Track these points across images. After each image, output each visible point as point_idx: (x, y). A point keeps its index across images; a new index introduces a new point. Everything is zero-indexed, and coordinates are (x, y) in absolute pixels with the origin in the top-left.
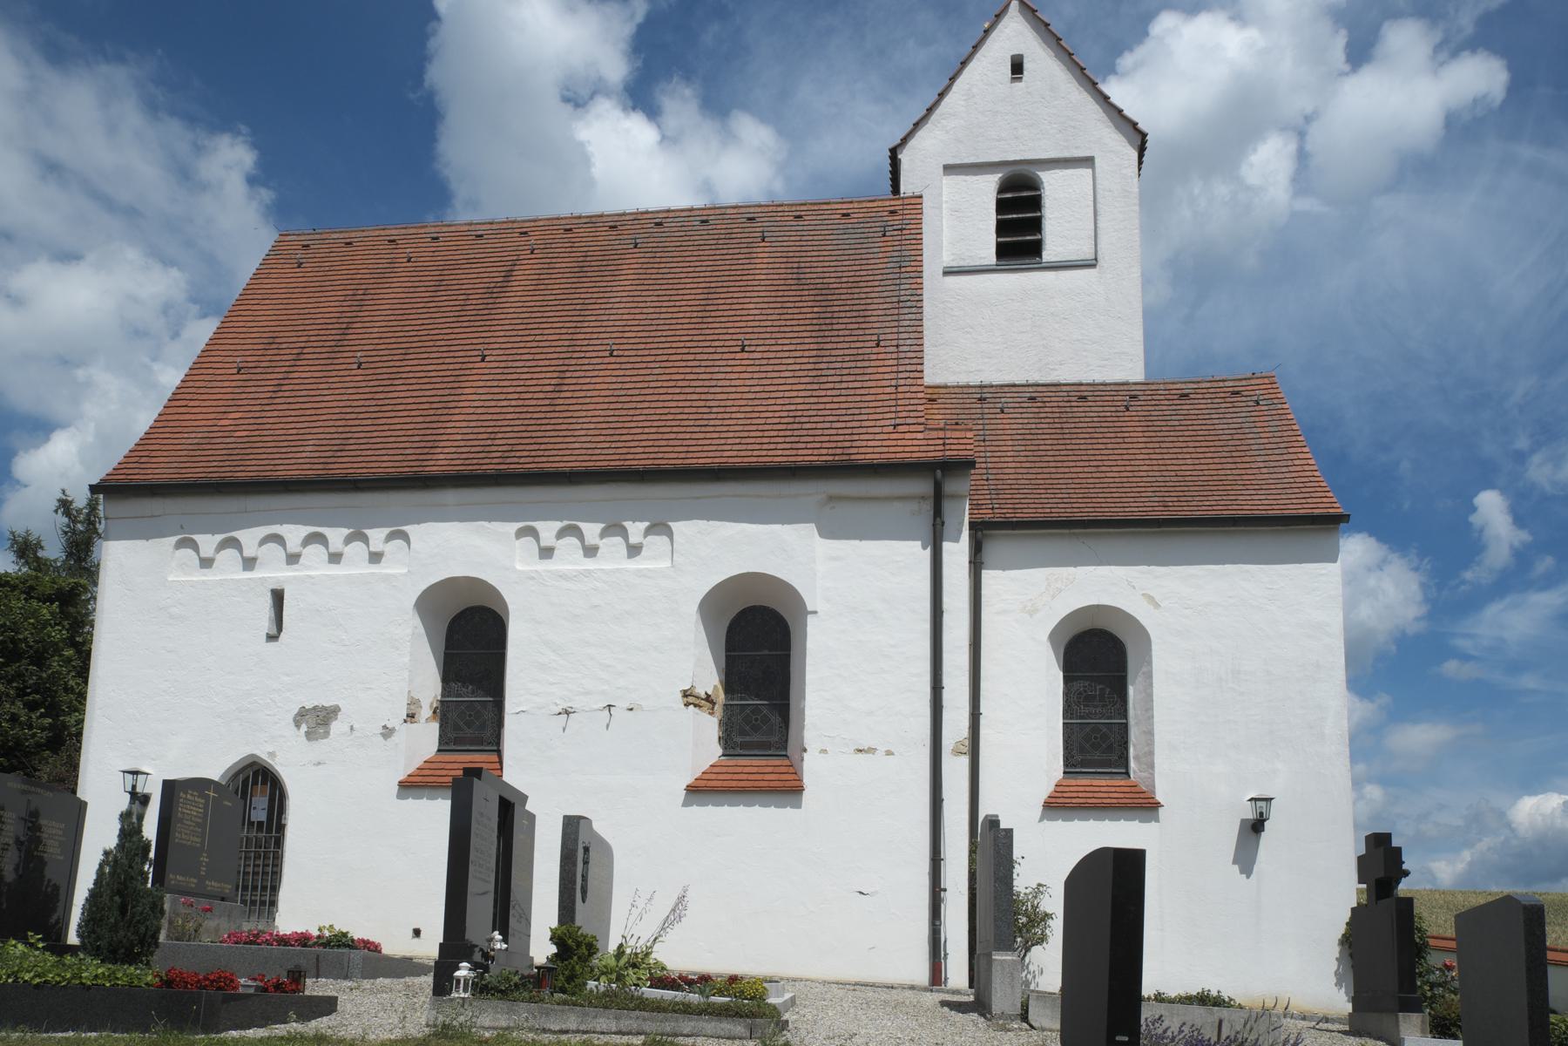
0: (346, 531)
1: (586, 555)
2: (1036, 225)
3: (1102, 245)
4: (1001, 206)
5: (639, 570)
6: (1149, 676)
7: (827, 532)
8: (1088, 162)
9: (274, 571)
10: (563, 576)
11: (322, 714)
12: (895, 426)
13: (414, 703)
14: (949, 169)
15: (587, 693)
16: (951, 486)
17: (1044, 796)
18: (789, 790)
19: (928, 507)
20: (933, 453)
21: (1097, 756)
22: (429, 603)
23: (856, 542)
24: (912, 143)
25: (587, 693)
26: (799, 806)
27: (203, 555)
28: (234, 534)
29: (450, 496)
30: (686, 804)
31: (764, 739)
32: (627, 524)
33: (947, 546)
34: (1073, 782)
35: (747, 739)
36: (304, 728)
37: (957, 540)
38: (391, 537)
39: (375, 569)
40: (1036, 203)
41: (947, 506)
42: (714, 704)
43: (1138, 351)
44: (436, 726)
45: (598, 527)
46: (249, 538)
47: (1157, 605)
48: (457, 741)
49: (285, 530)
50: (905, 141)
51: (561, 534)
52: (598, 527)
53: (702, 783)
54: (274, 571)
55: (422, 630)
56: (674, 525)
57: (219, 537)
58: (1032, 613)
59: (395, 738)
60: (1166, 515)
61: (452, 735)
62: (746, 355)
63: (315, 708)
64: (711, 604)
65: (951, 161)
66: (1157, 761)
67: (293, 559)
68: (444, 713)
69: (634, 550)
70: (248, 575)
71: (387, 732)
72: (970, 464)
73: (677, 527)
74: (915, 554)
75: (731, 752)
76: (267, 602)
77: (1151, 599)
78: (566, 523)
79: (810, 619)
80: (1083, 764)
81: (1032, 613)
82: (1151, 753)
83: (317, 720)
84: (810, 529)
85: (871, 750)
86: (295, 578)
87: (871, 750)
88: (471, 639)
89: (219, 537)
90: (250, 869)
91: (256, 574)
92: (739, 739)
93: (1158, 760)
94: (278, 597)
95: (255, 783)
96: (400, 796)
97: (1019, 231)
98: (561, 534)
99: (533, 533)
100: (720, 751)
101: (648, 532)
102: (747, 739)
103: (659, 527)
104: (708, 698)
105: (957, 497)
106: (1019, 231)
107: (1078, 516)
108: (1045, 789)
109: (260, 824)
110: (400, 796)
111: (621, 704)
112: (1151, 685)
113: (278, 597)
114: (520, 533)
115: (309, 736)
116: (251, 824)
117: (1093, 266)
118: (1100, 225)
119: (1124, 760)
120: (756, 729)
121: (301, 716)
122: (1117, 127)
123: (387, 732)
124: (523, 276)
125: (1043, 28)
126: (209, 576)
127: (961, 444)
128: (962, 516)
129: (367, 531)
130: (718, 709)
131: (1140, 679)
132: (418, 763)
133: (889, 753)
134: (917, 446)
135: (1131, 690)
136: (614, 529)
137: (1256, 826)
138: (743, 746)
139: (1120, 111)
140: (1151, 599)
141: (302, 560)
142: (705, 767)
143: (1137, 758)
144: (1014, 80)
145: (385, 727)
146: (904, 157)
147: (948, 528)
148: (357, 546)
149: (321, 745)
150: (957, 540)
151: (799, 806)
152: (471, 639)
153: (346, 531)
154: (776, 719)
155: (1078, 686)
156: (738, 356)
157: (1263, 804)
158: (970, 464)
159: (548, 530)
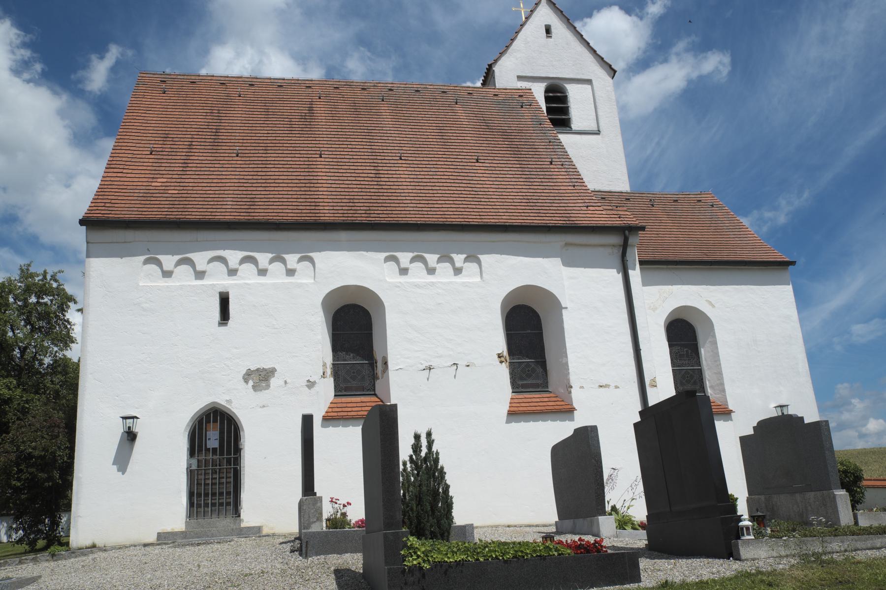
0: (270, 256)
1: (259, 274)
2: (565, 111)
5: (464, 283)
6: (715, 343)
7: (567, 263)
8: (589, 82)
9: (218, 280)
10: (417, 286)
11: (263, 374)
12: (587, 207)
15: (440, 357)
16: (633, 240)
17: (506, 412)
19: (618, 252)
23: (582, 269)
24: (500, 62)
25: (440, 357)
26: (573, 420)
27: (289, 267)
28: (311, 254)
29: (343, 236)
30: (507, 422)
31: (534, 382)
32: (454, 256)
33: (631, 272)
35: (525, 382)
36: (251, 383)
37: (634, 269)
38: (301, 260)
39: (290, 280)
40: (564, 99)
41: (629, 250)
43: (625, 178)
44: (332, 379)
45: (435, 257)
46: (201, 258)
47: (713, 306)
48: (346, 389)
49: (228, 254)
50: (496, 61)
51: (413, 260)
52: (435, 257)
54: (218, 280)
55: (324, 319)
56: (482, 257)
57: (177, 257)
61: (343, 385)
63: (258, 370)
67: (232, 272)
68: (337, 372)
69: (458, 271)
70: (199, 282)
71: (311, 384)
73: (483, 258)
74: (614, 276)
78: (416, 254)
79: (564, 311)
82: (722, 384)
83: (260, 378)
84: (557, 261)
85: (607, 386)
86: (236, 284)
87: (607, 386)
88: (354, 327)
89: (177, 257)
90: (210, 482)
91: (206, 282)
92: (521, 383)
93: (727, 387)
94: (224, 301)
95: (208, 422)
98: (413, 260)
99: (395, 259)
101: (466, 260)
102: (525, 382)
103: (472, 258)
107: (671, 258)
109: (214, 450)
111: (462, 363)
112: (717, 348)
113: (224, 301)
114: (387, 259)
115: (255, 388)
116: (208, 450)
117: (598, 134)
120: (529, 376)
121: (248, 375)
122: (601, 66)
123: (311, 384)
124: (320, 109)
125: (559, 12)
126: (459, 279)
127: (629, 219)
128: (634, 255)
129: (285, 256)
131: (708, 345)
133: (617, 387)
134: (601, 216)
135: (702, 351)
136: (445, 258)
137: (131, 436)
138: (523, 386)
139: (602, 59)
141: (239, 273)
143: (711, 387)
144: (548, 37)
145: (308, 381)
146: (496, 69)
147: (629, 264)
148: (278, 265)
149: (264, 395)
150: (634, 269)
152: (354, 327)
153: (270, 256)
154: (539, 370)
155: (676, 349)
156: (477, 164)
159: (405, 258)
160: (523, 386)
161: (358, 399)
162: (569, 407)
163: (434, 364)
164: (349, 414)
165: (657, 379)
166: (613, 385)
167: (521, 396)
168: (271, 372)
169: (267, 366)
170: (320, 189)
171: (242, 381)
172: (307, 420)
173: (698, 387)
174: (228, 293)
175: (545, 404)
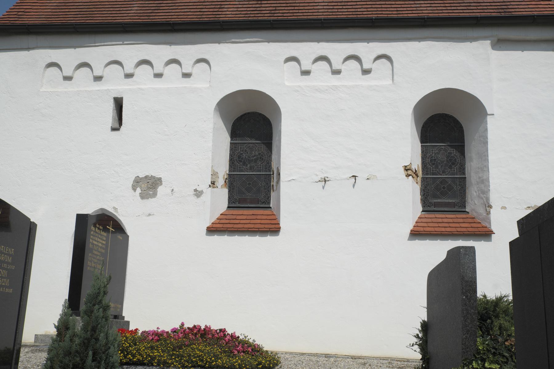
9: (115, 85)
11: (153, 180)
13: (214, 174)
18: (273, 229)
22: (226, 105)
26: (491, 241)
34: (240, 212)
36: (139, 190)
42: (418, 176)
44: (226, 191)
59: (203, 197)
63: (146, 177)
71: (198, 193)
76: (111, 106)
79: (489, 118)
83: (148, 186)
94: (119, 104)
96: (207, 235)
104: (416, 173)
113: (119, 104)
115: (143, 196)
119: (463, 204)
121: (137, 182)
123: (198, 193)
130: (419, 179)
132: (217, 215)
145: (196, 190)
151: (491, 241)
160: (436, 205)
161: (246, 212)
162: (277, 226)
163: (330, 176)
164: (236, 226)
167: (432, 215)
168: (196, 190)
169: (157, 175)
171: (131, 188)
174: (122, 98)
175: (457, 225)
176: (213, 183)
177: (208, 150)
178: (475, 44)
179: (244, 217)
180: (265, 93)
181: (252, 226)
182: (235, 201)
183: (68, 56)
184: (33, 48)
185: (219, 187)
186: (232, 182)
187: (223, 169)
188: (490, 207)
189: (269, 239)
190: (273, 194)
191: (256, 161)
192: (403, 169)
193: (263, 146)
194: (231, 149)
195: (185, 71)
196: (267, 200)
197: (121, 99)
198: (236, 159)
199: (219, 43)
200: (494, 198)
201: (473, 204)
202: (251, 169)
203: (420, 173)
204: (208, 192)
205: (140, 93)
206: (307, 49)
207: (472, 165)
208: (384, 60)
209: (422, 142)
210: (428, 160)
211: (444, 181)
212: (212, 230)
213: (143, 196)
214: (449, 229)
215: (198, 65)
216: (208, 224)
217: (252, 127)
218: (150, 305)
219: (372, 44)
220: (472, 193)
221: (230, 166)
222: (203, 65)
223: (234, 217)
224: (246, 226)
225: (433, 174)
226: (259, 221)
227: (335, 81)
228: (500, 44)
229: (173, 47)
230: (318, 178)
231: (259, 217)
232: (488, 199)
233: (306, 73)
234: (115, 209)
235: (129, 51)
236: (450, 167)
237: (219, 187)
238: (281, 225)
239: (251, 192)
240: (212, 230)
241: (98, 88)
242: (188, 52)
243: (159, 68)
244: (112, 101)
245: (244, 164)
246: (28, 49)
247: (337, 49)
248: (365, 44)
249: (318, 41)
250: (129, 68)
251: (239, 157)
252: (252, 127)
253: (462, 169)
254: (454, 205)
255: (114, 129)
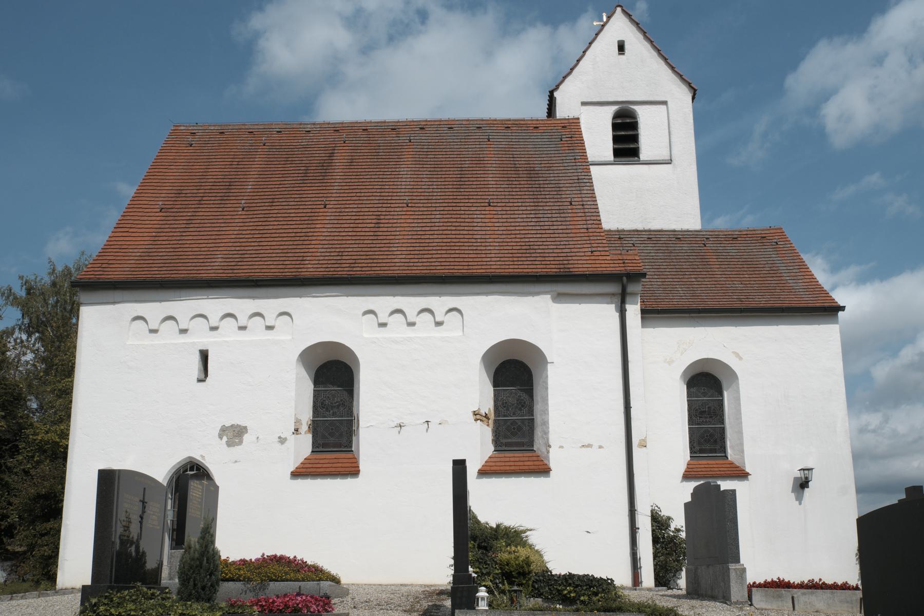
2: (635, 139)
3: (674, 152)
4: (615, 127)
8: (664, 103)
9: (201, 338)
11: (238, 429)
13: (298, 422)
14: (584, 104)
16: (631, 288)
18: (353, 471)
20: (617, 268)
21: (708, 447)
22: (307, 356)
29: (118, 294)
36: (225, 439)
40: (634, 126)
44: (310, 436)
47: (741, 358)
48: (324, 445)
50: (557, 87)
53: (488, 468)
58: (670, 362)
60: (743, 306)
62: (492, 208)
63: (232, 426)
64: (488, 357)
65: (585, 100)
66: (745, 449)
72: (644, 275)
75: (500, 448)
76: (196, 359)
77: (737, 355)
79: (549, 365)
80: (701, 451)
81: (670, 362)
82: (742, 444)
83: (234, 434)
85: (589, 446)
87: (589, 446)
92: (504, 441)
94: (204, 356)
97: (626, 141)
100: (493, 448)
104: (486, 416)
105: (634, 294)
106: (626, 141)
108: (682, 468)
110: (478, 477)
111: (434, 422)
112: (739, 404)
113: (204, 356)
115: (230, 444)
118: (672, 140)
119: (724, 449)
121: (224, 431)
123: (282, 441)
124: (340, 160)
130: (491, 422)
132: (301, 460)
133: (600, 447)
134: (608, 263)
138: (507, 445)
140: (737, 355)
142: (486, 458)
143: (732, 447)
145: (280, 438)
156: (487, 208)
157: (806, 472)
158: (644, 275)
160: (507, 445)
161: (328, 456)
165: (648, 440)
166: (596, 445)
167: (502, 455)
169: (243, 423)
170: (313, 242)
172: (459, 467)
173: (718, 447)
174: (207, 351)
176: (297, 430)
177: (294, 397)
178: (537, 298)
179: (327, 461)
180: (344, 345)
181: (333, 470)
182: (319, 445)
183: (154, 309)
184: (119, 303)
185: (303, 433)
186: (316, 428)
187: (307, 415)
188: (550, 446)
189: (349, 482)
190: (354, 438)
191: (338, 407)
192: (472, 414)
193: (345, 393)
194: (314, 396)
195: (268, 324)
196: (349, 444)
197: (207, 351)
198: (319, 406)
199: (301, 297)
200: (553, 439)
201: (538, 445)
202: (334, 414)
203: (492, 416)
204: (292, 439)
205: (225, 344)
206: (384, 302)
207: (538, 408)
208: (455, 313)
209: (494, 386)
210: (500, 403)
211: (514, 422)
212: (296, 475)
213: (230, 444)
214: (513, 468)
215: (280, 317)
216: (292, 469)
217: (333, 375)
218: (236, 541)
219: (444, 298)
220: (538, 433)
221: (314, 412)
222: (286, 318)
223: (317, 461)
224: (328, 470)
225: (505, 416)
226: (340, 465)
227: (410, 332)
228: (559, 297)
229: (257, 301)
230: (395, 424)
231: (340, 461)
232: (548, 439)
233: (383, 325)
234: (203, 457)
235: (214, 305)
236: (520, 410)
237: (303, 433)
238: (361, 468)
239: (333, 439)
240: (296, 475)
241: (183, 341)
242: (271, 305)
243: (243, 321)
244: (198, 353)
245: (327, 410)
246: (114, 303)
247: (411, 303)
248: (438, 298)
249: (394, 295)
250: (214, 322)
251: (322, 403)
252: (333, 375)
253: (531, 412)
254: (523, 444)
255: (199, 381)
